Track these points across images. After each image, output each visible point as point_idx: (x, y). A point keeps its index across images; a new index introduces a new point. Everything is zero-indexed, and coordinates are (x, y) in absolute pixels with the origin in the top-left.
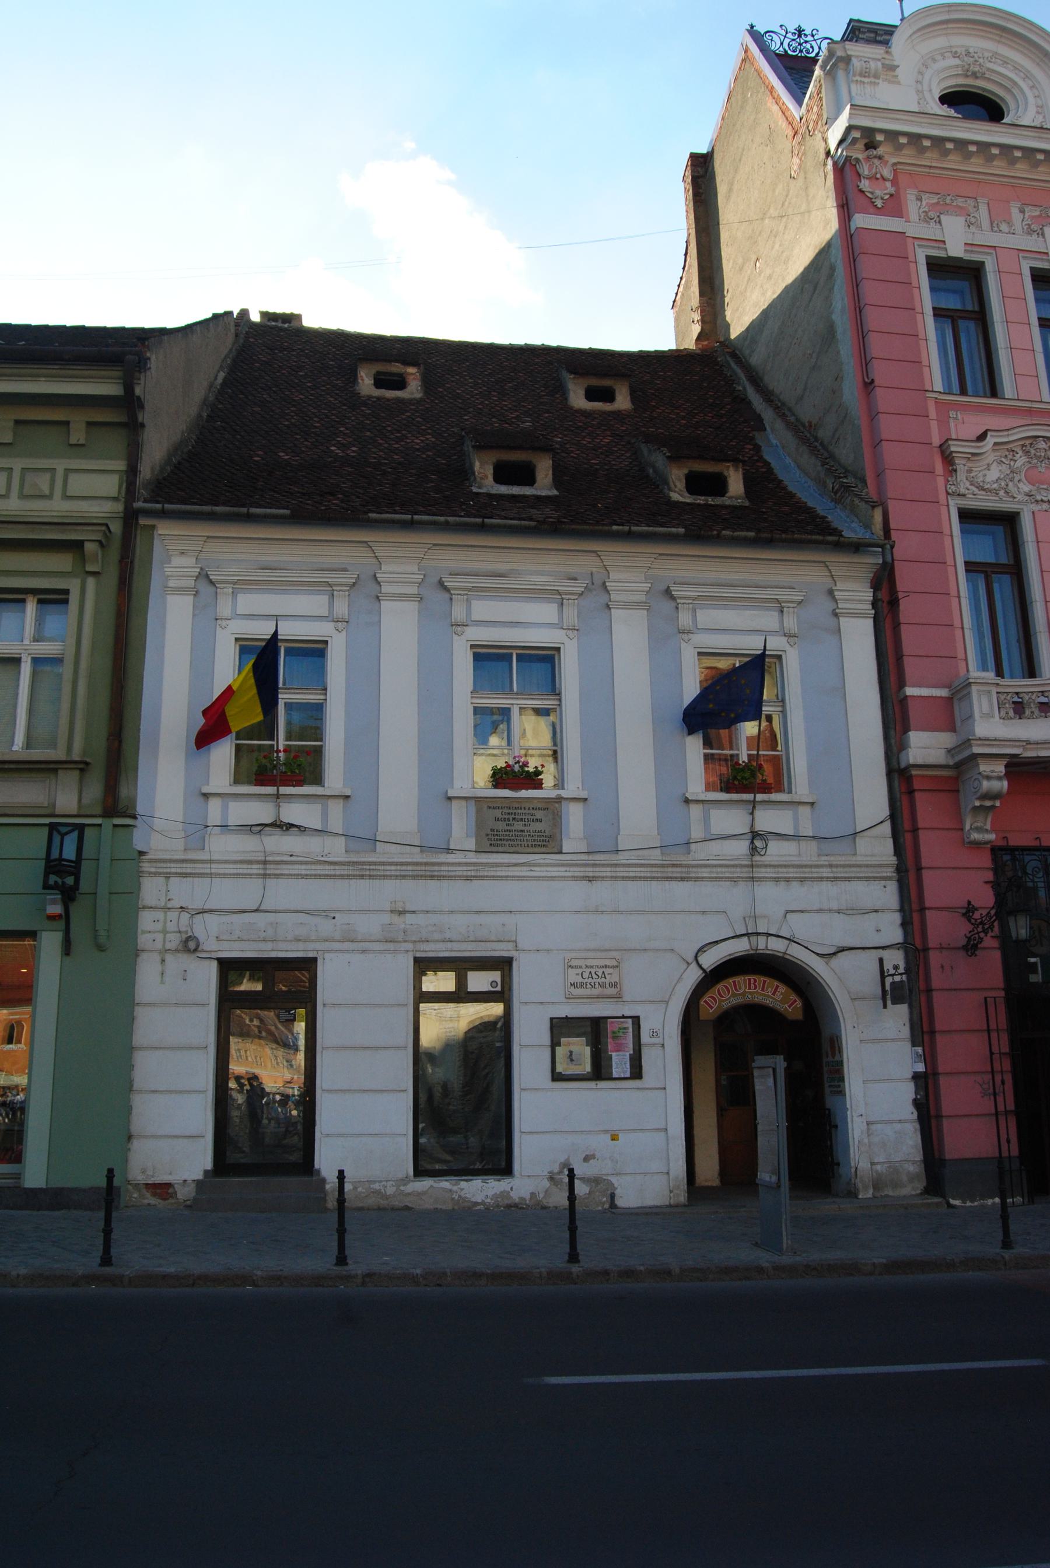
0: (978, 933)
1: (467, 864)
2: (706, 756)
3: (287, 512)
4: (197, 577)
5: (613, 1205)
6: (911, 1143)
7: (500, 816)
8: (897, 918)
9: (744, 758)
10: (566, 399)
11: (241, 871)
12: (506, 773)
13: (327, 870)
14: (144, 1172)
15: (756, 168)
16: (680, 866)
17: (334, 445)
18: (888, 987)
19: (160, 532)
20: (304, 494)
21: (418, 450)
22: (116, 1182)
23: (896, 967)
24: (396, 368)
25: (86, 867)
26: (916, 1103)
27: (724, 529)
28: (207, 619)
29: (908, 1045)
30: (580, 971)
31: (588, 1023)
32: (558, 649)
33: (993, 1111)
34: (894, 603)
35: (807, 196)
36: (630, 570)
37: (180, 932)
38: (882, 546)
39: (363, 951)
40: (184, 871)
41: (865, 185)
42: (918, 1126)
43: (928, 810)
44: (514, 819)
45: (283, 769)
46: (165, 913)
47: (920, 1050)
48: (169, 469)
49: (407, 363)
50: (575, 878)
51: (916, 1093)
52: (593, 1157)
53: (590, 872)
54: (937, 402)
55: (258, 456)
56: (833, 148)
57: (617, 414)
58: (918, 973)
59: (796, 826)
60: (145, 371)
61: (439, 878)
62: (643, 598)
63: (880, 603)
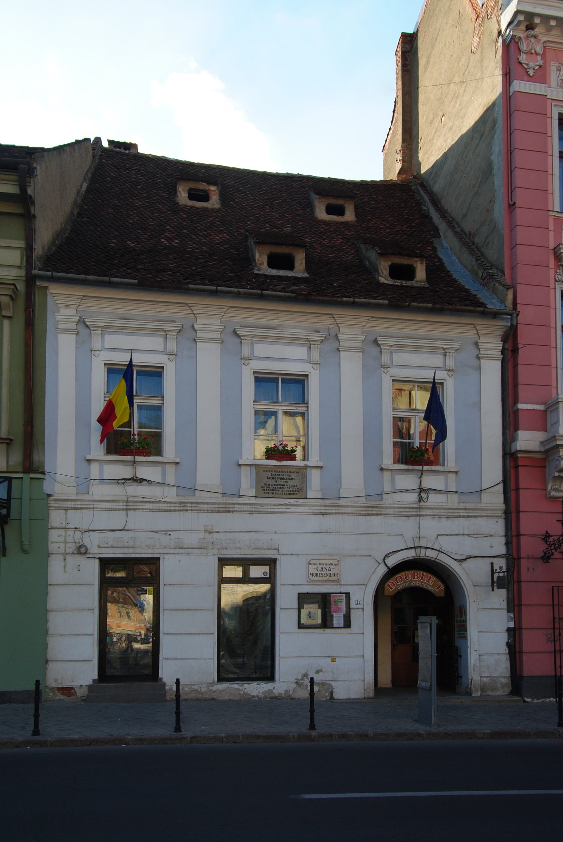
0: (551, 550)
1: (250, 504)
2: (394, 442)
3: (136, 281)
4: (77, 322)
5: (332, 697)
6: (504, 666)
7: (270, 476)
8: (503, 540)
9: (417, 444)
10: (313, 213)
11: (112, 507)
12: (274, 451)
13: (165, 506)
14: (56, 681)
15: (447, 44)
16: (377, 507)
17: (163, 238)
18: (495, 579)
19: (51, 291)
20: (145, 270)
21: (218, 244)
22: (41, 687)
23: (501, 568)
24: (203, 186)
25: (14, 504)
26: (508, 645)
27: (413, 302)
28: (85, 351)
29: (505, 612)
30: (316, 567)
31: (320, 596)
32: (307, 376)
33: (553, 650)
34: (515, 351)
35: (482, 67)
36: (353, 326)
37: (75, 543)
38: (511, 315)
39: (188, 554)
40: (77, 506)
41: (523, 58)
42: (508, 657)
43: (526, 478)
44: (278, 478)
45: (137, 445)
46: (66, 531)
47: (512, 615)
48: (54, 249)
49: (209, 183)
50: (314, 513)
51: (508, 639)
52: (321, 671)
53: (323, 509)
54: (556, 219)
55: (113, 243)
56: (503, 28)
57: (346, 224)
58: (513, 572)
59: (446, 485)
60: (33, 177)
61: (234, 512)
62: (360, 345)
63: (506, 351)
